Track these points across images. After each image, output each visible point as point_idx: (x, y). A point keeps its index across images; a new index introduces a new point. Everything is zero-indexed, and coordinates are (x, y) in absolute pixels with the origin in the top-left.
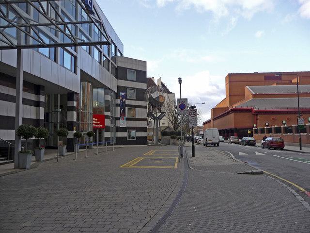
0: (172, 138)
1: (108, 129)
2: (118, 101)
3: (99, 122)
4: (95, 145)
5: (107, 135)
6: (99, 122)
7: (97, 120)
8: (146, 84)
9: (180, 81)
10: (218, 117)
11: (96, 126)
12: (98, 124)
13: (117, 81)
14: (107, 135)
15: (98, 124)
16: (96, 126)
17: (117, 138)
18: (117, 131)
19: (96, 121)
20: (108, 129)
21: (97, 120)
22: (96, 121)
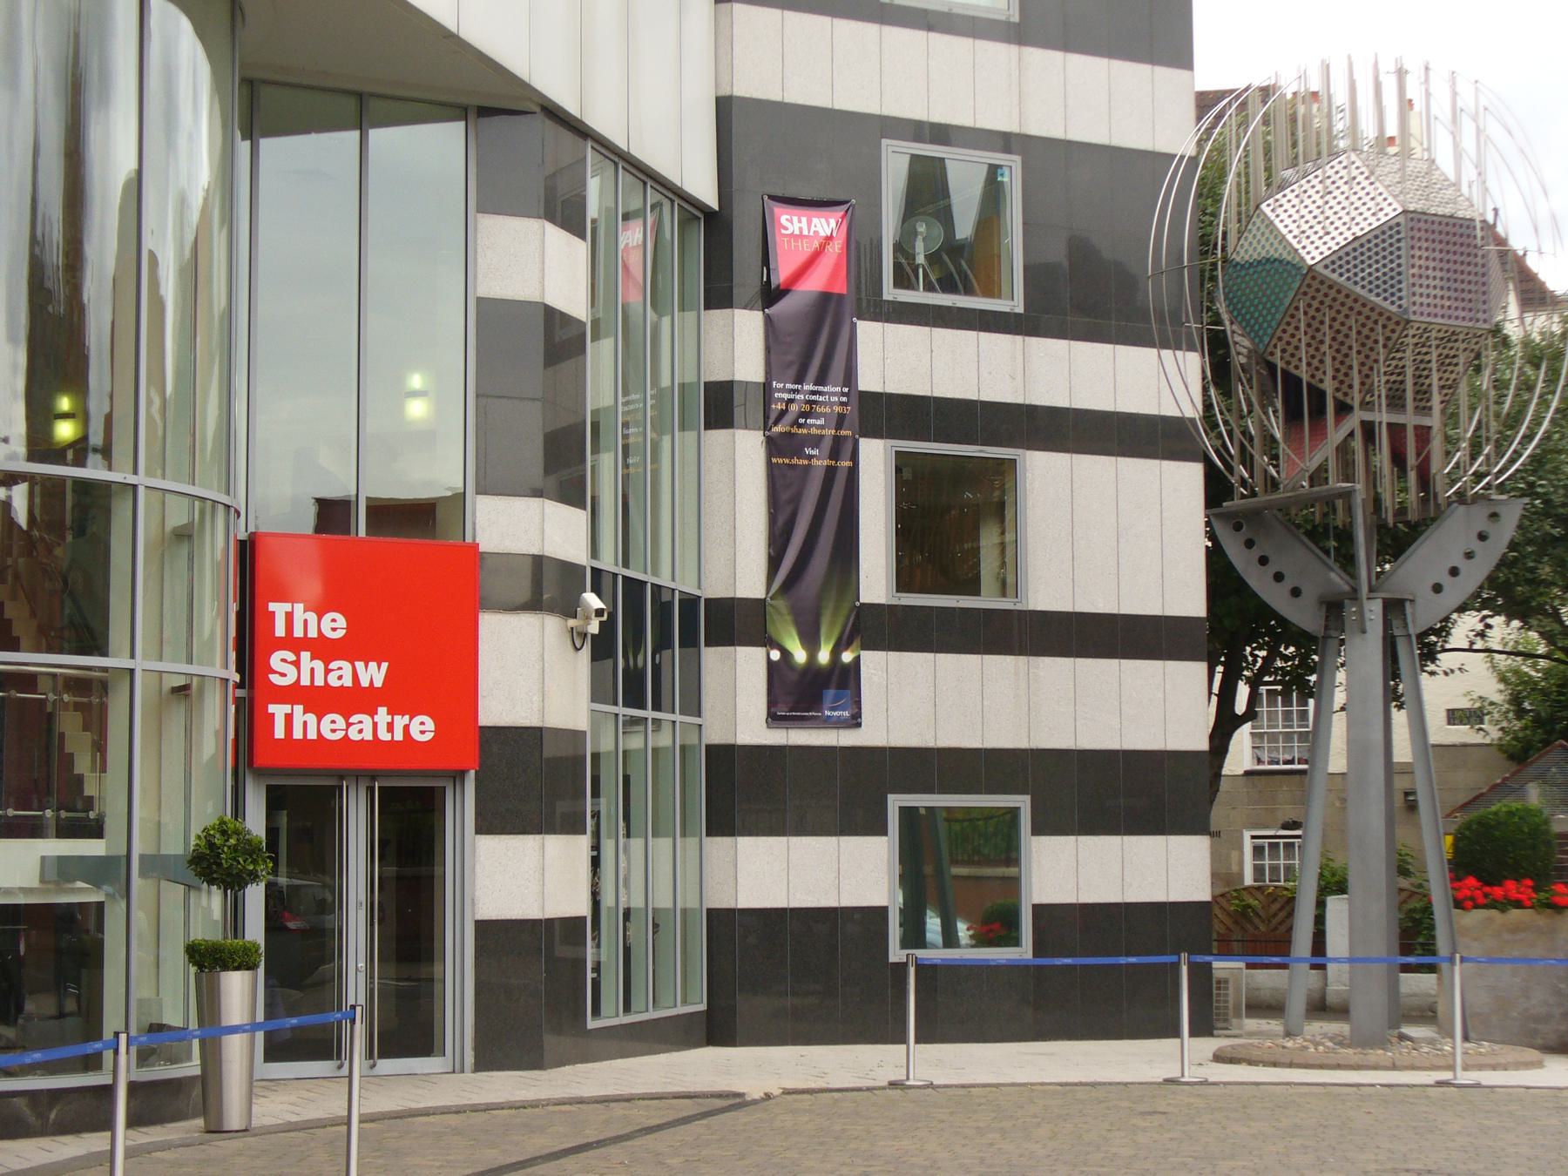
0: (1250, 966)
1: (535, 783)
2: (739, 345)
3: (374, 674)
4: (299, 1040)
5: (511, 876)
6: (374, 674)
7: (334, 625)
8: (1192, 364)
9: (1427, 69)
10: (428, 1115)
11: (332, 727)
12: (354, 700)
13: (722, 40)
14: (511, 876)
15: (354, 700)
16: (332, 727)
17: (723, 922)
18: (723, 822)
19: (324, 649)
20: (535, 783)
21: (334, 625)
22: (324, 649)
